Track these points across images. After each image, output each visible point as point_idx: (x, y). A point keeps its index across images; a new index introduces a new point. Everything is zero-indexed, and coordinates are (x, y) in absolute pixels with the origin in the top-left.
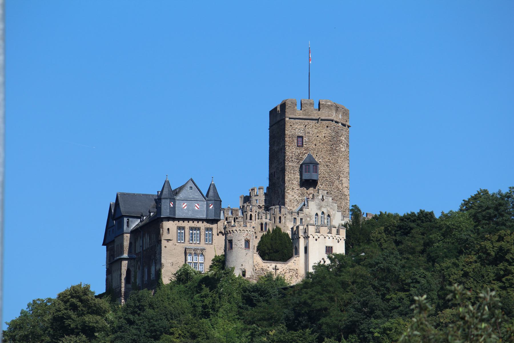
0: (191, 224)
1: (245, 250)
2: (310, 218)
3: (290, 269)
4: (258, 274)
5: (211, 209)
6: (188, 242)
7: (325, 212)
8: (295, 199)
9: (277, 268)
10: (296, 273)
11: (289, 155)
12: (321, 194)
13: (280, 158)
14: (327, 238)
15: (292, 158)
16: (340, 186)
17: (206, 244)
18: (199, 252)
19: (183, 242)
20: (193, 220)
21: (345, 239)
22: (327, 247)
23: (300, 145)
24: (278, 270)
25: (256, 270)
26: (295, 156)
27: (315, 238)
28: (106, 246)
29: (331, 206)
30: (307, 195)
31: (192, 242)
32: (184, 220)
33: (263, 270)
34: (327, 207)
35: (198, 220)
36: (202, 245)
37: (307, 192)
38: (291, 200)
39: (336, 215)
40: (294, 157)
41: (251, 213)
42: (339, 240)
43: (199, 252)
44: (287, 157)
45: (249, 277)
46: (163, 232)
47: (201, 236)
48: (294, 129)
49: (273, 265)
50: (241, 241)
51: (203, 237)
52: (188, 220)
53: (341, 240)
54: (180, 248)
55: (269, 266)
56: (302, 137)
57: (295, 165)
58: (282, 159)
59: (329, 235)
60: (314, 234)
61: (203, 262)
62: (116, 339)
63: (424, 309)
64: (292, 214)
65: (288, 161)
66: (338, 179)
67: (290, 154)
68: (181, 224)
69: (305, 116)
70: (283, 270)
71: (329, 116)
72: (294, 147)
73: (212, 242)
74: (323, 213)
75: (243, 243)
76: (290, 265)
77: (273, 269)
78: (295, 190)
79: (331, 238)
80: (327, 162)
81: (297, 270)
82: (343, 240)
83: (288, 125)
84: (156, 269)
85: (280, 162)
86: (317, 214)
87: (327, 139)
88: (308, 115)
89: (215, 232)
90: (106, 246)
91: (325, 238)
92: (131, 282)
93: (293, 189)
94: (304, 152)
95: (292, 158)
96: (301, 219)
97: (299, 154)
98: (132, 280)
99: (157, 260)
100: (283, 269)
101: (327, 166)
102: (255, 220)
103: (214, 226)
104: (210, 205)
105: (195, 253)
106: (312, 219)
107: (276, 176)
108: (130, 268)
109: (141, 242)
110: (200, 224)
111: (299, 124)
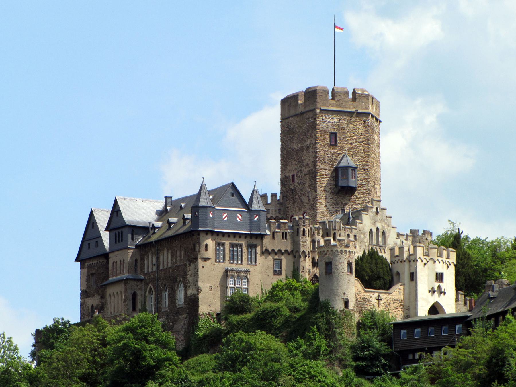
1: (347, 275)
2: (364, 235)
3: (394, 300)
5: (255, 221)
7: (380, 227)
9: (380, 298)
11: (321, 156)
14: (437, 262)
15: (324, 159)
18: (242, 274)
21: (455, 264)
22: (437, 273)
23: (334, 144)
24: (381, 301)
28: (80, 263)
30: (342, 206)
34: (382, 222)
36: (244, 267)
37: (342, 202)
39: (391, 232)
42: (449, 265)
43: (242, 274)
44: (318, 157)
45: (352, 308)
46: (200, 248)
48: (326, 124)
57: (328, 168)
59: (440, 259)
60: (423, 258)
62: (235, 381)
64: (345, 230)
65: (319, 163)
67: (322, 155)
68: (221, 240)
69: (339, 107)
70: (387, 301)
72: (326, 146)
74: (377, 229)
76: (394, 295)
77: (376, 299)
79: (441, 262)
82: (452, 265)
83: (320, 118)
84: (186, 294)
85: (305, 164)
86: (371, 231)
87: (364, 137)
88: (343, 106)
90: (80, 263)
94: (338, 152)
95: (324, 159)
96: (354, 235)
100: (387, 299)
101: (365, 170)
104: (255, 216)
105: (238, 276)
107: (296, 180)
110: (243, 242)
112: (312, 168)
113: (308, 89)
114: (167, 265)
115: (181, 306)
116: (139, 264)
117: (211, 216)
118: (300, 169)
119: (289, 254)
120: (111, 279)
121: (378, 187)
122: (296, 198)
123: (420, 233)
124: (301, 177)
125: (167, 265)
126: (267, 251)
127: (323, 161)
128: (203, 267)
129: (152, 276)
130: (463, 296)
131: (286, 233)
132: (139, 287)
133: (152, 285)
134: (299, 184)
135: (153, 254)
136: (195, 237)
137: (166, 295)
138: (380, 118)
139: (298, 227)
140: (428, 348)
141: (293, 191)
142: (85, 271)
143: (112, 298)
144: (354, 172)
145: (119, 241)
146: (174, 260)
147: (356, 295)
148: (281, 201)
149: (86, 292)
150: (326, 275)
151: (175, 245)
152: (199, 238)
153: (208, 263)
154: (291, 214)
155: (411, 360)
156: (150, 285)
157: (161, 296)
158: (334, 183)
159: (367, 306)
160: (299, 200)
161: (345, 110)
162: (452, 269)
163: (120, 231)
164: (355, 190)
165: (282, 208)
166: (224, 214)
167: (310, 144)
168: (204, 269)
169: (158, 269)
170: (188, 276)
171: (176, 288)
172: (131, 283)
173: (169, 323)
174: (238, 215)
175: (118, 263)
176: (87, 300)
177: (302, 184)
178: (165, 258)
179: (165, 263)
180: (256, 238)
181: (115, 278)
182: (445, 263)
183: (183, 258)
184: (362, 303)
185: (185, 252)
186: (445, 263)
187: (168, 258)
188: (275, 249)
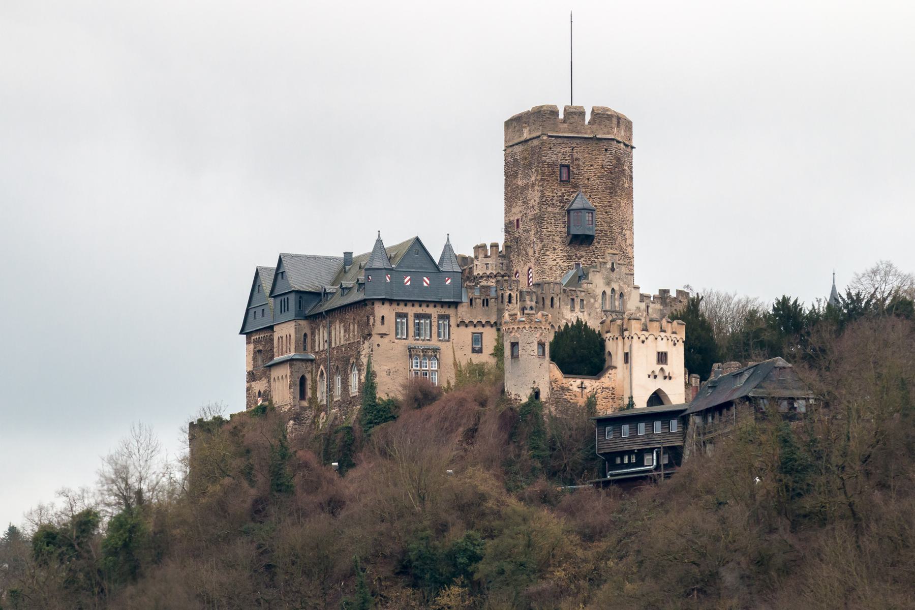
0: (418, 309)
2: (595, 299)
3: (603, 388)
4: (556, 396)
5: (447, 285)
6: (413, 338)
7: (616, 288)
8: (558, 265)
9: (583, 387)
10: (612, 394)
12: (610, 260)
13: (530, 200)
14: (659, 339)
15: (552, 200)
16: (623, 245)
17: (440, 341)
19: (404, 337)
20: (420, 303)
21: (684, 340)
22: (659, 353)
25: (553, 389)
26: (557, 196)
27: (641, 339)
29: (625, 280)
31: (417, 338)
32: (406, 302)
33: (563, 390)
35: (428, 303)
36: (434, 343)
37: (576, 254)
38: (551, 268)
40: (555, 198)
41: (510, 292)
42: (676, 342)
45: (545, 400)
46: (374, 322)
47: (433, 328)
49: (579, 381)
50: (532, 345)
51: (435, 329)
52: (413, 303)
53: (678, 341)
54: (400, 346)
55: (572, 382)
56: (568, 166)
57: (557, 211)
58: (535, 201)
59: (663, 334)
60: (639, 333)
61: (436, 369)
63: (430, 398)
66: (620, 233)
68: (402, 309)
71: (609, 133)
73: (449, 338)
74: (613, 290)
75: (535, 347)
77: (579, 388)
78: (558, 252)
79: (665, 339)
80: (606, 206)
81: (613, 389)
82: (681, 342)
85: (530, 205)
86: (604, 293)
87: (606, 169)
89: (453, 322)
91: (656, 339)
92: (307, 397)
93: (554, 249)
94: (572, 190)
95: (552, 200)
97: (563, 193)
98: (309, 393)
99: (361, 366)
101: (606, 212)
102: (517, 303)
103: (450, 311)
105: (424, 355)
106: (597, 301)
108: (306, 375)
109: (326, 335)
110: (431, 310)
111: (563, 145)
112: (537, 211)
113: (533, 108)
114: (340, 342)
115: (354, 395)
116: (309, 340)
117: (389, 280)
118: (525, 212)
119: (492, 326)
120: (277, 359)
121: (628, 233)
122: (520, 250)
123: (673, 294)
124: (526, 222)
125: (340, 342)
126: (462, 322)
127: (550, 202)
128: (378, 345)
129: (324, 356)
130: (699, 380)
131: (487, 300)
132: (309, 369)
133: (324, 367)
134: (524, 231)
135: (324, 327)
136: (368, 308)
137: (338, 380)
138: (634, 145)
139: (502, 292)
140: (638, 450)
141: (517, 240)
142: (252, 346)
143: (285, 380)
144: (590, 215)
145: (285, 311)
146: (347, 336)
147: (551, 383)
148: (504, 253)
149: (253, 373)
150: (512, 358)
151: (347, 317)
152: (373, 309)
153: (386, 340)
154: (515, 270)
155: (619, 464)
156: (322, 367)
157: (333, 381)
158: (566, 230)
159: (565, 397)
160: (524, 252)
161: (580, 135)
162: (680, 349)
163: (286, 297)
164: (593, 240)
165: (505, 262)
166: (407, 277)
167: (536, 180)
168: (380, 348)
169: (329, 347)
170: (362, 357)
171: (349, 372)
172: (299, 364)
173: (341, 415)
174: (425, 278)
175: (284, 339)
176: (253, 384)
177: (527, 231)
178: (338, 333)
179: (338, 340)
180: (449, 307)
181: (280, 357)
182: (670, 340)
183: (356, 333)
184: (558, 392)
185: (359, 326)
186: (670, 340)
187: (340, 333)
188: (473, 320)
